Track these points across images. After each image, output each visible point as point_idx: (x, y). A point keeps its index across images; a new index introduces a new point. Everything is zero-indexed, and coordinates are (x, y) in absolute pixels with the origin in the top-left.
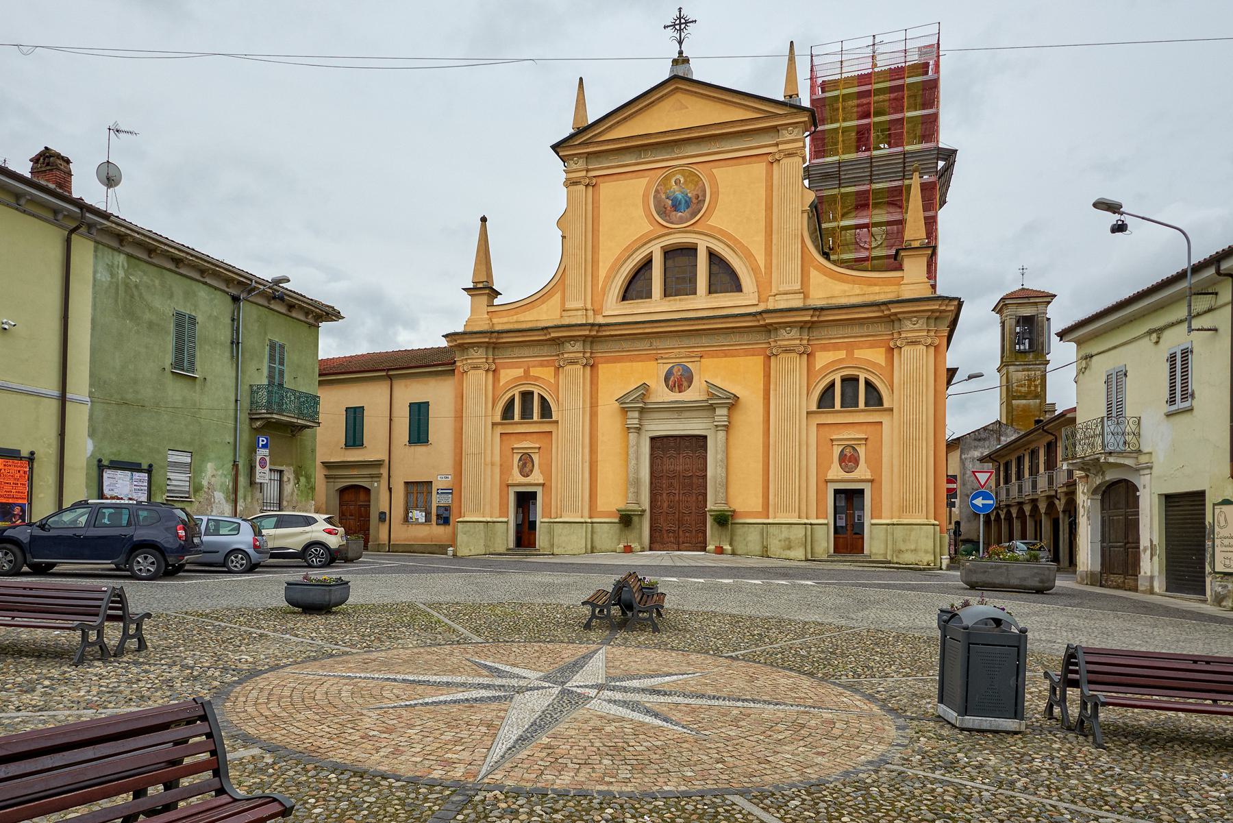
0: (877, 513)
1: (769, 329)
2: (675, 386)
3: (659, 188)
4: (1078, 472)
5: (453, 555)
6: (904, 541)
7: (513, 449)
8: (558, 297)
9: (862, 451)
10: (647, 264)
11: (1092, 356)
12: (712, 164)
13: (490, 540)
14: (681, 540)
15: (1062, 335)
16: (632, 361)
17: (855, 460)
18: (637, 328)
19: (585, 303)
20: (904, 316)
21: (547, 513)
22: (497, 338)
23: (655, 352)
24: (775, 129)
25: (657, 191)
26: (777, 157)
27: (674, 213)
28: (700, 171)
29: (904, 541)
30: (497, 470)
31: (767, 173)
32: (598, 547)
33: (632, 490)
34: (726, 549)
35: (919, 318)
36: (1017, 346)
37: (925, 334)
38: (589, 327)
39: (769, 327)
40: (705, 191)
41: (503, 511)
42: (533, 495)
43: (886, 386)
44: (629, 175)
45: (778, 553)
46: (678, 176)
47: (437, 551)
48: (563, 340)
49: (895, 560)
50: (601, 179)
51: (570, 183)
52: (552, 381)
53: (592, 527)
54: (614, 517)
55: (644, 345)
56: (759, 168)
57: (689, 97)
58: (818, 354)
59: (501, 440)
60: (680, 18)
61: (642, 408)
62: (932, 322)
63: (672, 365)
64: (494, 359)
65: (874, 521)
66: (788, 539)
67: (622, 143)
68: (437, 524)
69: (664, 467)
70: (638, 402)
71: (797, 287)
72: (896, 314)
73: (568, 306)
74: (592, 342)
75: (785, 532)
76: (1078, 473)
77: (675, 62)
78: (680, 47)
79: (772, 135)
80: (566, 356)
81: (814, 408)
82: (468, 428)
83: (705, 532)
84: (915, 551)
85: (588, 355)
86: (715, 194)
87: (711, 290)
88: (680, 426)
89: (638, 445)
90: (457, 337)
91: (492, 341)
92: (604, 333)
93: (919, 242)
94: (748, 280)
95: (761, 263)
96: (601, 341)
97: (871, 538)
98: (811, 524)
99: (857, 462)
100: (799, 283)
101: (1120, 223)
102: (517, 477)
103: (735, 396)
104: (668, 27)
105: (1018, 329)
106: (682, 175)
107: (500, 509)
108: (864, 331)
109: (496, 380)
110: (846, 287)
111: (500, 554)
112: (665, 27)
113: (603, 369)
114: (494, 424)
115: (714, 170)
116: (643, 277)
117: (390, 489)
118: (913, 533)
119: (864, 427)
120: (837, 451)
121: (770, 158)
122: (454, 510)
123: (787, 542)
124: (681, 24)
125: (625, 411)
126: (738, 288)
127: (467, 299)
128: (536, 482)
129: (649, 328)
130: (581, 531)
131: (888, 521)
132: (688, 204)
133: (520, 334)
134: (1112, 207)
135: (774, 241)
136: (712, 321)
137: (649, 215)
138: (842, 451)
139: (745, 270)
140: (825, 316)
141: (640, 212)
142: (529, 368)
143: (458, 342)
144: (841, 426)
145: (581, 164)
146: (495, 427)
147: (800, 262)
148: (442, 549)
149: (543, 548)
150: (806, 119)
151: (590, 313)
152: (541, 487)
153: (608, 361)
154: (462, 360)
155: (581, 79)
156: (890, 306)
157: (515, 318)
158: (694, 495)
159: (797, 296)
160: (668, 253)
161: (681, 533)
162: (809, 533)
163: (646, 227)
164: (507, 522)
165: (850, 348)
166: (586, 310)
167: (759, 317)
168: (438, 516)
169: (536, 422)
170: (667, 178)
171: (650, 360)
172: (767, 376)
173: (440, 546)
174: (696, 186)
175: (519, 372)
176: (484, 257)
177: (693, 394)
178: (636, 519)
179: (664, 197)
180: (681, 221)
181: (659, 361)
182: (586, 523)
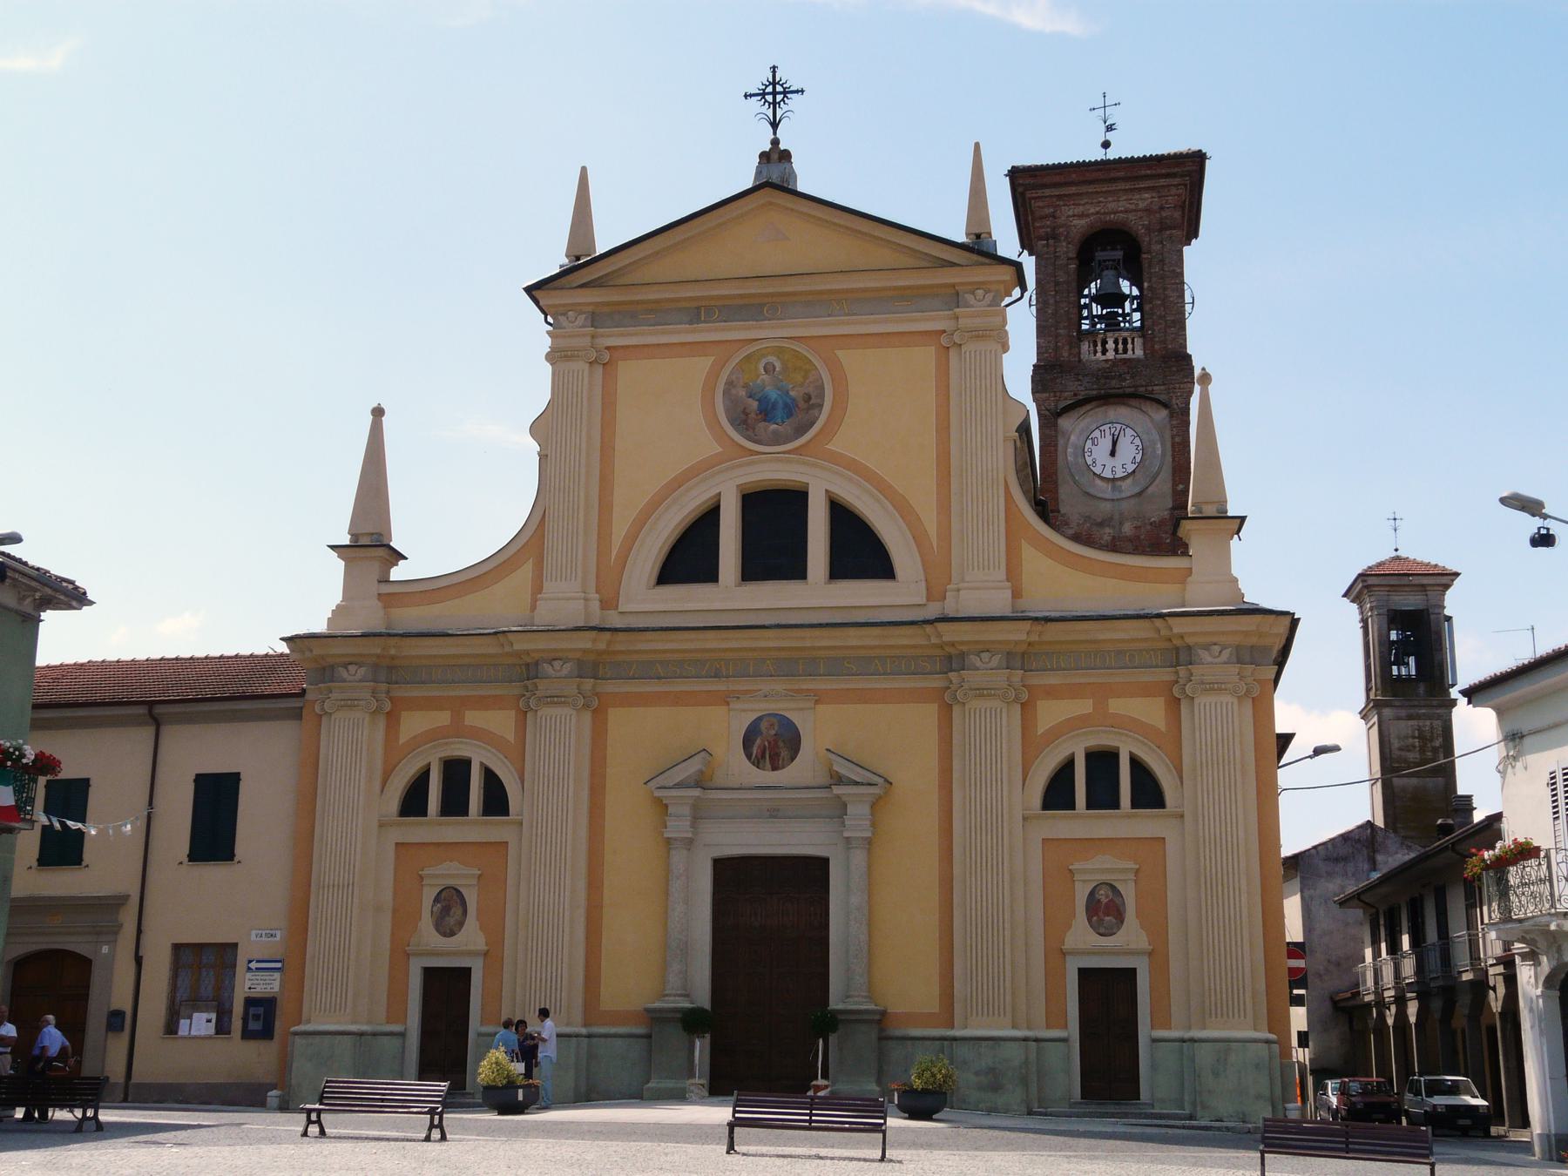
2: (763, 756)
4: (1517, 945)
6: (1216, 1074)
11: (1522, 737)
15: (1472, 694)
27: (763, 424)
36: (1395, 668)
40: (822, 388)
46: (772, 359)
59: (397, 858)
60: (774, 83)
76: (1518, 947)
77: (764, 156)
78: (775, 133)
95: (932, 530)
98: (1037, 1040)
99: (1120, 918)
101: (1543, 532)
103: (886, 780)
104: (751, 95)
105: (1393, 636)
113: (618, 719)
117: (139, 961)
124: (775, 93)
132: (790, 409)
134: (1530, 506)
137: (713, 423)
138: (1092, 894)
150: (1008, 278)
162: (1033, 1056)
163: (709, 447)
164: (402, 1035)
177: (801, 770)
179: (742, 393)
182: (578, 1036)
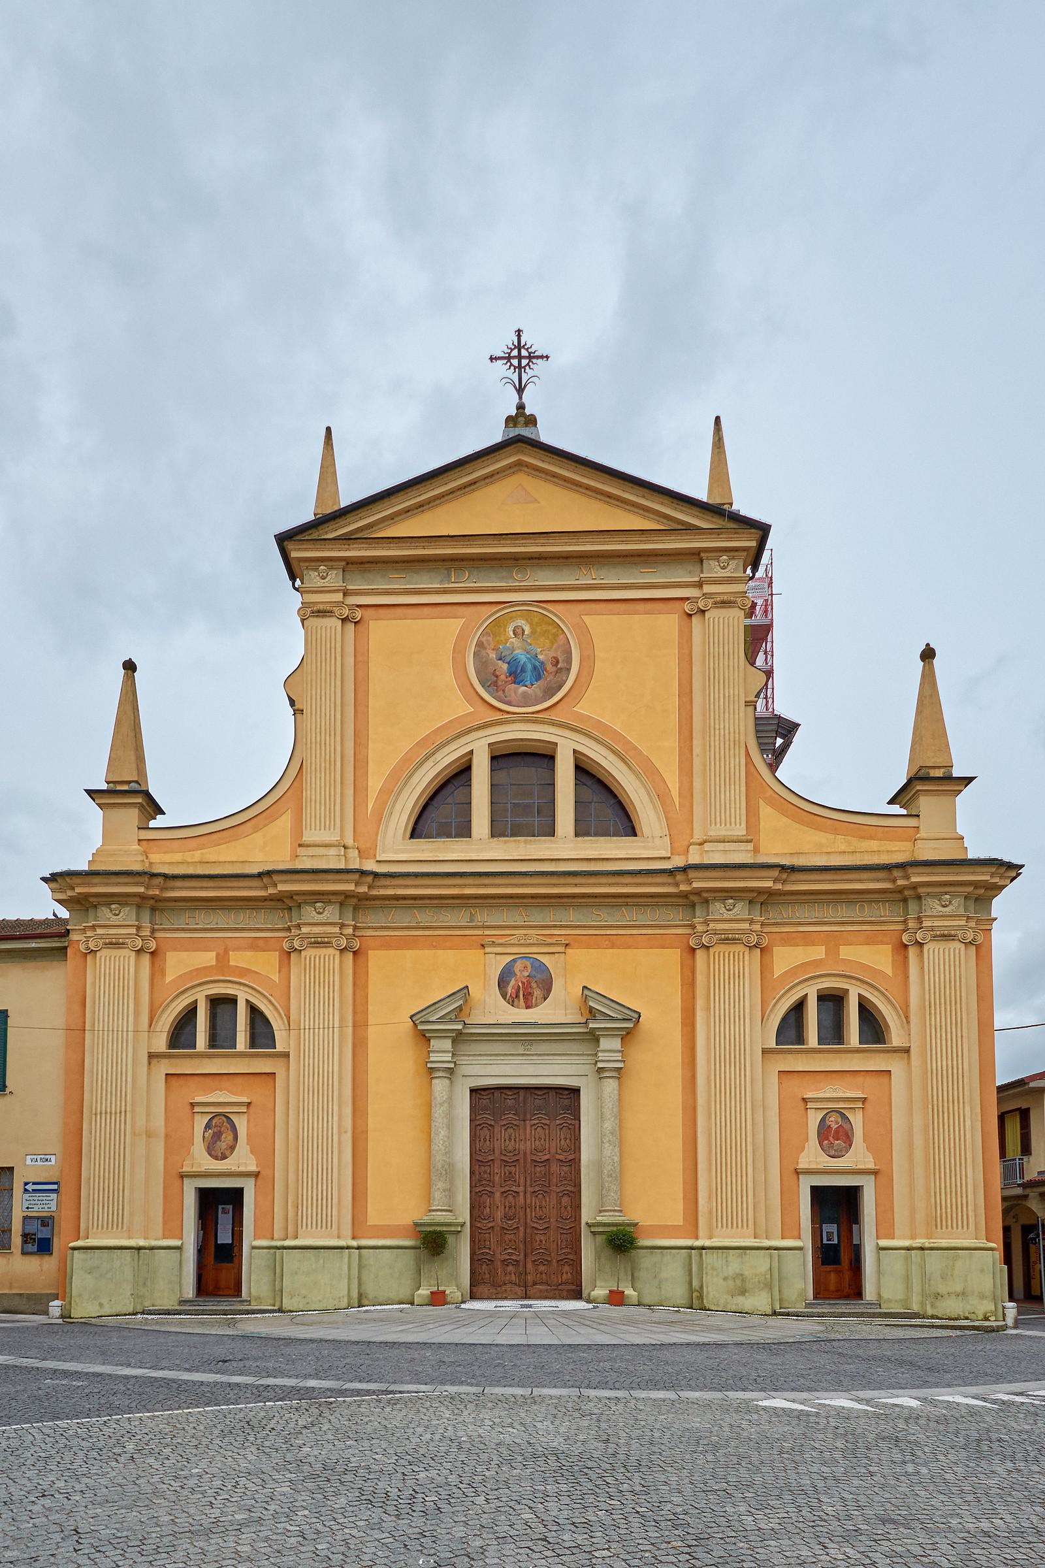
0: (886, 1228)
1: (692, 901)
2: (518, 996)
3: (484, 639)
5: (62, 1317)
6: (943, 1277)
7: (192, 1105)
8: (285, 822)
9: (857, 1120)
10: (462, 773)
12: (582, 606)
13: (144, 1284)
14: (530, 1278)
16: (435, 947)
17: (846, 1136)
18: (449, 886)
19: (342, 835)
20: (929, 890)
21: (265, 1228)
22: (163, 889)
23: (480, 932)
24: (697, 557)
25: (480, 645)
26: (701, 605)
28: (565, 618)
29: (943, 1277)
30: (159, 1148)
31: (680, 631)
32: (371, 1296)
33: (440, 1185)
34: (628, 1297)
35: (954, 895)
37: (963, 923)
38: (356, 876)
39: (692, 898)
40: (569, 653)
41: (172, 1226)
42: (235, 1197)
43: (898, 1013)
44: (426, 610)
45: (722, 1302)
46: (521, 622)
47: (23, 1308)
48: (298, 898)
49: (930, 1312)
50: (371, 611)
51: (311, 613)
52: (276, 978)
53: (360, 1256)
54: (406, 1237)
55: (459, 917)
56: (669, 622)
57: (542, 483)
58: (777, 950)
59: (780, 1083)
61: (459, 1033)
62: (971, 903)
63: (511, 958)
64: (153, 931)
65: (883, 1243)
66: (740, 1276)
67: (416, 548)
68: (24, 1253)
69: (497, 1144)
70: (451, 1021)
71: (740, 831)
72: (914, 887)
73: (307, 837)
74: (356, 908)
75: (734, 1264)
77: (511, 421)
78: (520, 398)
79: (690, 567)
80: (305, 930)
81: (772, 1044)
82: (97, 1061)
83: (576, 1264)
84: (963, 1294)
85: (350, 931)
86: (589, 660)
87: (581, 830)
88: (531, 1070)
89: (450, 1100)
90: (77, 880)
91: (151, 892)
92: (382, 892)
93: (942, 770)
94: (652, 814)
96: (373, 908)
97: (879, 1272)
99: (848, 1139)
100: (744, 825)
102: (201, 1160)
106: (527, 620)
107: (164, 1223)
108: (855, 913)
109: (157, 972)
110: (822, 838)
111: (168, 1312)
112: (491, 359)
113: (377, 959)
114: (152, 1056)
115: (586, 618)
116: (449, 800)
118: (959, 1264)
119: (860, 1079)
120: (814, 1119)
121: (687, 607)
122: (64, 1226)
123: (738, 1282)
125: (424, 1037)
126: (630, 829)
127: (94, 814)
128: (242, 1169)
129: (470, 886)
130: (341, 1264)
131: (906, 1243)
132: (538, 672)
133: (211, 883)
135: (697, 750)
136: (592, 880)
138: (823, 1120)
139: (645, 798)
140: (794, 882)
141: (447, 678)
142: (226, 951)
143: (78, 890)
144: (818, 1077)
145: (334, 579)
146: (154, 1061)
147: (743, 789)
148: (38, 1303)
149: (258, 1298)
151: (354, 854)
152: (252, 1181)
153: (387, 944)
154: (84, 930)
155: (328, 430)
156: (910, 870)
157: (197, 856)
158: (554, 1196)
159: (743, 846)
160: (501, 758)
161: (529, 1266)
162: (775, 1264)
163: (461, 708)
165: (833, 942)
166: (345, 847)
167: (679, 877)
168: (27, 1237)
169: (242, 1055)
170: (498, 624)
171: (471, 947)
172: (689, 984)
173: (30, 1297)
174: (552, 643)
175: (208, 958)
176: (132, 734)
178: (451, 1239)
179: (493, 655)
180: (526, 701)
181: (488, 950)
182: (348, 1248)
